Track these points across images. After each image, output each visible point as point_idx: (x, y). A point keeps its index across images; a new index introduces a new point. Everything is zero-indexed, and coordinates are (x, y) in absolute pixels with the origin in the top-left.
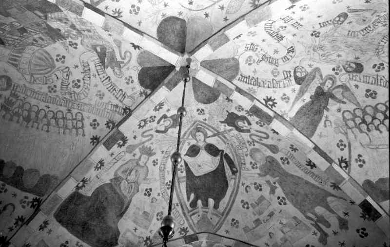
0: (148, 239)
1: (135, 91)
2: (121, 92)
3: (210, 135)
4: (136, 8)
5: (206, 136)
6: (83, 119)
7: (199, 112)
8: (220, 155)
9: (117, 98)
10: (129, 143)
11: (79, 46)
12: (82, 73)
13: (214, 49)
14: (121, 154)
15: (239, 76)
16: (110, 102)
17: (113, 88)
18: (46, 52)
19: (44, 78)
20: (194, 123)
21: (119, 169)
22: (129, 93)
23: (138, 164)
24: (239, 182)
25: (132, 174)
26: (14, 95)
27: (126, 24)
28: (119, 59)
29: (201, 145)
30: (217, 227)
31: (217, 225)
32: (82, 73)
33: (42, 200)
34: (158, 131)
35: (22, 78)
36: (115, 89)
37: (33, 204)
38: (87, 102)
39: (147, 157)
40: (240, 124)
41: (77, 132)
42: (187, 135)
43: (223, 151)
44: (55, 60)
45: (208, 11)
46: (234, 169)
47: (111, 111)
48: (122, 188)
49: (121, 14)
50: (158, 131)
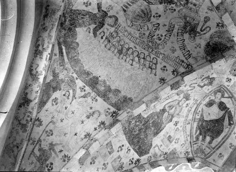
0: (166, 153)
2: (188, 52)
3: (226, 96)
5: (223, 96)
6: (156, 64)
7: (227, 80)
8: (225, 111)
9: (184, 56)
12: (166, 31)
14: (173, 94)
16: (179, 57)
17: (183, 48)
19: (139, 26)
20: (220, 86)
22: (194, 54)
24: (232, 131)
29: (216, 101)
30: (208, 156)
31: (208, 154)
32: (166, 31)
33: (119, 113)
34: (199, 86)
35: (125, 21)
36: (184, 49)
37: (112, 115)
38: (162, 52)
42: (212, 92)
43: (229, 109)
44: (153, 15)
46: (232, 122)
47: (178, 63)
48: (164, 117)
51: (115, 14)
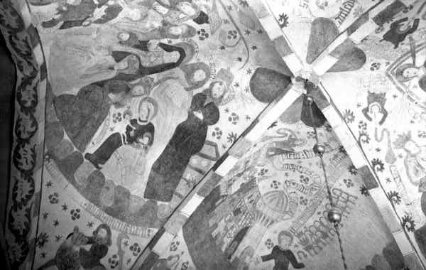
1: (324, 134)
4: (232, 117)
5: (413, 65)
7: (375, 68)
10: (383, 159)
11: (265, 168)
13: (290, 51)
15: (337, 22)
18: (265, 195)
20: (389, 76)
21: (409, 177)
23: (414, 156)
25: (422, 165)
26: (299, 235)
27: (244, 135)
28: (286, 138)
34: (381, 123)
39: (410, 142)
40: (403, 29)
41: (351, 202)
42: (402, 87)
45: (250, 46)
49: (234, 134)
50: (381, 123)
51: (277, 236)
